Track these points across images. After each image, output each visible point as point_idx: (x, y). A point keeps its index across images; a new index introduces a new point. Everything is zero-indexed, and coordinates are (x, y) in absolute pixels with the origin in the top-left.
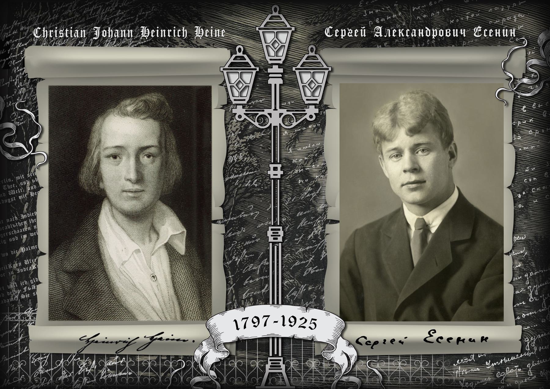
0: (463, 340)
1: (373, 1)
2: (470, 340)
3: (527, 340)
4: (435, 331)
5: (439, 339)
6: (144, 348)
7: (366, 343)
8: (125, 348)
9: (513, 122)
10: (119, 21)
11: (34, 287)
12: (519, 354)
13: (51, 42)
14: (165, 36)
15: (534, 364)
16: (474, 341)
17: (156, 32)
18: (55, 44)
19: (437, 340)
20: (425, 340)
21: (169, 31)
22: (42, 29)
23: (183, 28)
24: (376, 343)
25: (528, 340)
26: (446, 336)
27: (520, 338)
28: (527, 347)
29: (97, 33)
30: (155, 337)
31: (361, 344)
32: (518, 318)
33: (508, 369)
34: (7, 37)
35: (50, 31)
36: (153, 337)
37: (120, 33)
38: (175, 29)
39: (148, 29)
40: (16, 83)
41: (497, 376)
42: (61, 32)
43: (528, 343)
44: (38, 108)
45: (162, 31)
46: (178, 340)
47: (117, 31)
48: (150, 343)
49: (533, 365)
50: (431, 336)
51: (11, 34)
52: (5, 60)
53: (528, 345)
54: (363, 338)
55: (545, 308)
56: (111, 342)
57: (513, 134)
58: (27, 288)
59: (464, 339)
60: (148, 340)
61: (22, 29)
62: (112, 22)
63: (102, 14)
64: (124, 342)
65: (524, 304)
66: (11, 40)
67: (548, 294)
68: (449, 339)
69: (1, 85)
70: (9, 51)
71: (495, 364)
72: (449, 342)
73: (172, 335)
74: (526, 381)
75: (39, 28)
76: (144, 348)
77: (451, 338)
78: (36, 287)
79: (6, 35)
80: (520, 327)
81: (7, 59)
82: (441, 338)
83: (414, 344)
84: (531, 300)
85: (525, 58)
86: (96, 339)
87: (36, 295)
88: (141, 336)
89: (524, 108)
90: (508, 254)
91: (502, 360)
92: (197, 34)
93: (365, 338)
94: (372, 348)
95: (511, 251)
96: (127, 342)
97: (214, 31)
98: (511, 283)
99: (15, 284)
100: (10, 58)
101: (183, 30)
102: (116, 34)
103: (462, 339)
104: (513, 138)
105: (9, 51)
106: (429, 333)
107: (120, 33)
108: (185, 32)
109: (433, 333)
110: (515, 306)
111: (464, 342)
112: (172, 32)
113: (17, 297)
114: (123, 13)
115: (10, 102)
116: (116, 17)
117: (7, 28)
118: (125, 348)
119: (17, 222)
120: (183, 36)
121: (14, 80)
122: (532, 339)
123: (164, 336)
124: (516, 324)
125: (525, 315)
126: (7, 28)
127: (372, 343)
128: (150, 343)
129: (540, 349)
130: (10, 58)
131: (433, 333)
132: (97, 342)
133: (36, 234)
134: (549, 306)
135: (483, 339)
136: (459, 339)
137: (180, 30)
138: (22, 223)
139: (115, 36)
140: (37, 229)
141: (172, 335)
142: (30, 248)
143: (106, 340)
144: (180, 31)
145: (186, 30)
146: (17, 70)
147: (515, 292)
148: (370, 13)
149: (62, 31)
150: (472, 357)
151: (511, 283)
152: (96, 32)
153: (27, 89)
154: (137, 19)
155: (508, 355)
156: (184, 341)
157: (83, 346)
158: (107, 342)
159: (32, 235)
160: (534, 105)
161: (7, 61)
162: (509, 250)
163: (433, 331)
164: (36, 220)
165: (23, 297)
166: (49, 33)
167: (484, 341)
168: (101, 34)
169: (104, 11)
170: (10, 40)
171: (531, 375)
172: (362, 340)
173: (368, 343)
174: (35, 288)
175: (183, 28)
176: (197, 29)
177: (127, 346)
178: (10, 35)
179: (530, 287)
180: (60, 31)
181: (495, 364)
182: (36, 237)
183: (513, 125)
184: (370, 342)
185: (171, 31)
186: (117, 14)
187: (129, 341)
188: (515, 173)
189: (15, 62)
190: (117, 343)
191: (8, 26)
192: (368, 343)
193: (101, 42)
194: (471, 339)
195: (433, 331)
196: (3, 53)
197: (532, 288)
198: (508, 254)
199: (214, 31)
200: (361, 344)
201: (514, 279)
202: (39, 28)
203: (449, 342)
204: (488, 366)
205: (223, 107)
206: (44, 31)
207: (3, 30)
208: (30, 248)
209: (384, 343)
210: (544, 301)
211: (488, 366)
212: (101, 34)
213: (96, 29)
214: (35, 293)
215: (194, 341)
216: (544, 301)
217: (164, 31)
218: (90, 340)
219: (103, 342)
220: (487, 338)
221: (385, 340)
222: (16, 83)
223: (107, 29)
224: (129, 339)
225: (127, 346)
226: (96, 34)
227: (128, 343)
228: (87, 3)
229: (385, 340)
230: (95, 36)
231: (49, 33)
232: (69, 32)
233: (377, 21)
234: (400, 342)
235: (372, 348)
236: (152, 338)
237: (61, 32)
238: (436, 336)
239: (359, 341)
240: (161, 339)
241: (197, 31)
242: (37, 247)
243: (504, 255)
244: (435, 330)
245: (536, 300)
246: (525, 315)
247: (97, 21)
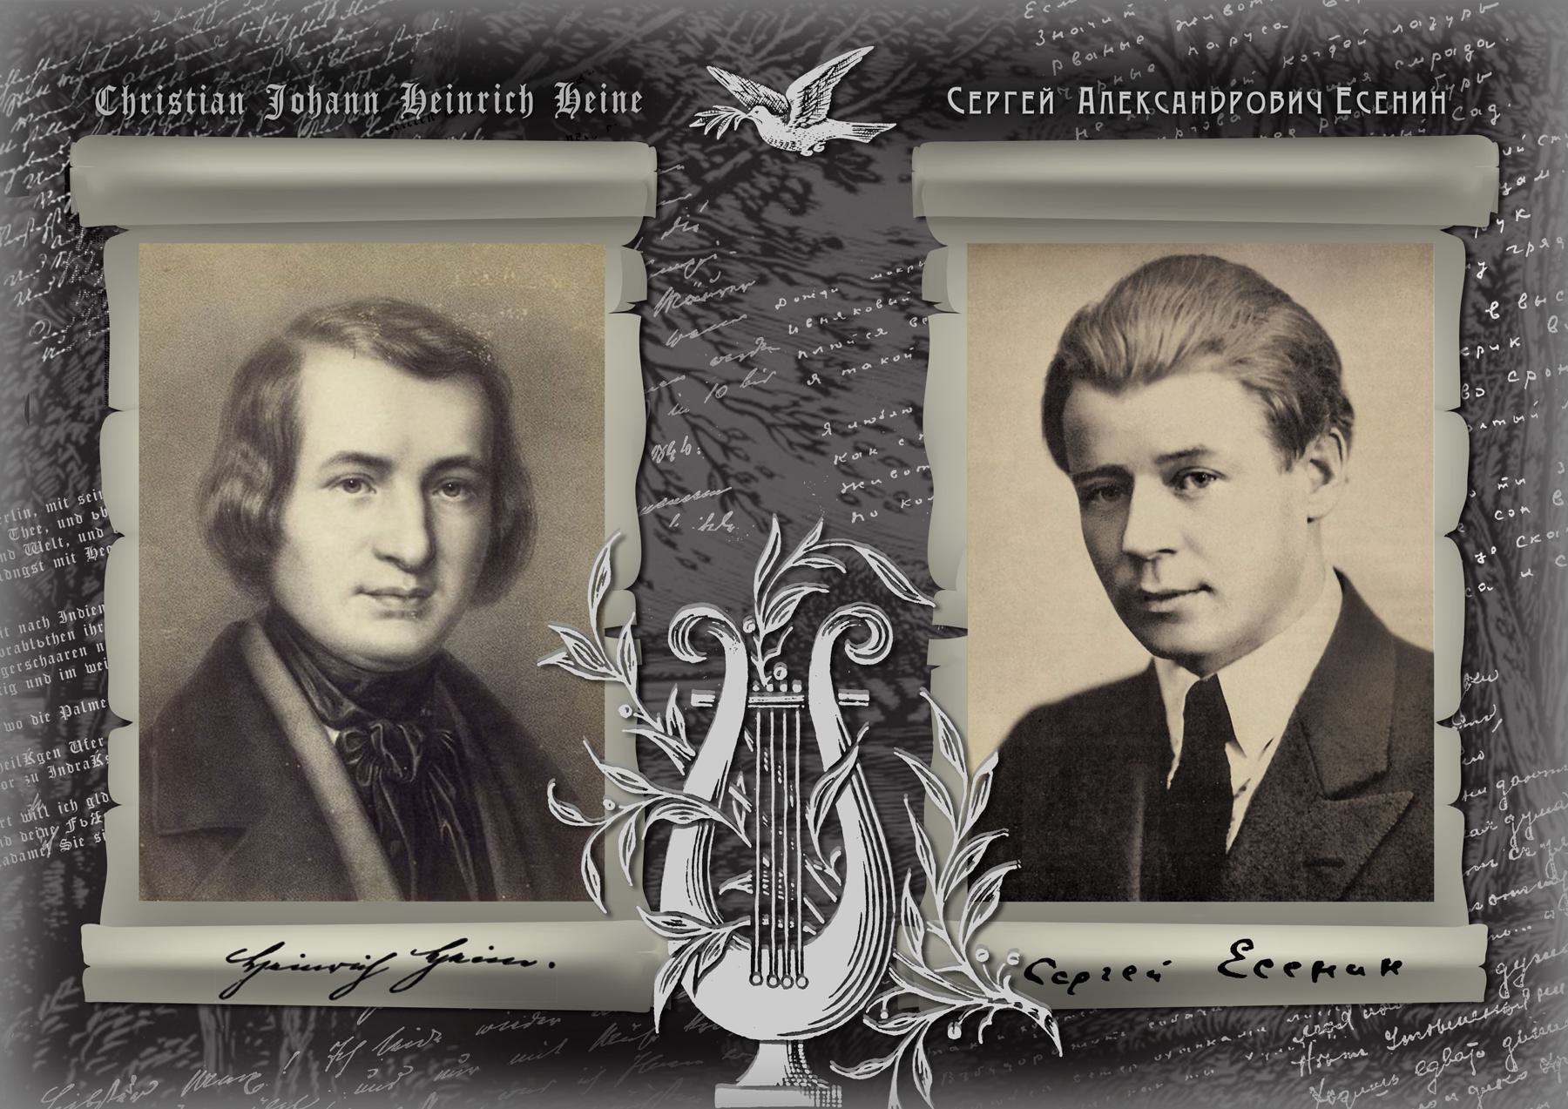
0: (1331, 970)
1: (1064, 4)
2: (1350, 969)
3: (1502, 968)
4: (1250, 945)
5: (1263, 968)
6: (411, 986)
7: (1055, 979)
8: (356, 983)
9: (1461, 348)
10: (340, 61)
11: (98, 817)
12: (1482, 1005)
13: (141, 125)
14: (469, 110)
15: (1523, 1039)
16: (1361, 971)
17: (444, 98)
18: (157, 125)
19: (1257, 969)
20: (1222, 968)
21: (481, 95)
22: (120, 91)
23: (523, 88)
24: (1083, 977)
25: (1505, 970)
26: (1281, 956)
27: (1482, 961)
28: (1503, 990)
29: (277, 102)
30: (442, 954)
31: (1038, 980)
32: (1479, 907)
33: (1447, 1052)
34: (19, 104)
35: (143, 96)
36: (436, 953)
37: (341, 101)
38: (499, 91)
39: (421, 92)
40: (45, 236)
41: (1417, 1072)
42: (174, 99)
43: (1506, 978)
44: (107, 308)
45: (461, 95)
46: (507, 961)
47: (335, 95)
48: (429, 969)
49: (1520, 1041)
50: (1239, 957)
51: (31, 95)
52: (13, 171)
53: (1505, 983)
54: (1046, 964)
55: (1554, 877)
56: (318, 968)
57: (1462, 384)
58: (77, 820)
59: (1333, 968)
60: (423, 962)
61: (62, 82)
62: (320, 63)
63: (290, 39)
64: (355, 966)
65: (1493, 865)
66: (32, 115)
67: (1563, 839)
68: (1290, 968)
69: (4, 241)
70: (26, 144)
71: (1412, 1038)
72: (1291, 975)
73: (491, 948)
74: (1499, 1087)
75: (112, 89)
76: (411, 986)
77: (1296, 965)
78: (102, 819)
79: (17, 99)
80: (1481, 929)
81: (20, 168)
82: (1268, 963)
83: (1192, 977)
84: (1515, 854)
85: (1497, 170)
86: (273, 958)
87: (103, 842)
88: (404, 954)
89: (1493, 308)
90: (1447, 723)
91: (1431, 1027)
92: (560, 104)
93: (1052, 963)
94: (1070, 992)
95: (1456, 716)
96: (361, 968)
97: (609, 96)
98: (1459, 804)
99: (42, 811)
100: (27, 164)
101: (522, 93)
102: (331, 106)
103: (1326, 966)
104: (1463, 394)
105: (26, 144)
106: (1234, 949)
107: (341, 101)
108: (527, 99)
109: (1244, 949)
110: (1468, 873)
111: (1363, 974)
112: (492, 98)
113: (48, 846)
114: (350, 37)
115: (30, 292)
116: (333, 47)
117: (21, 80)
118: (356, 983)
119: (48, 632)
120: (523, 110)
121: (39, 229)
122: (1516, 967)
123: (467, 951)
124: (1471, 922)
125: (1496, 899)
126: (21, 80)
127: (1071, 979)
128: (429, 969)
129: (1540, 996)
130: (27, 164)
131: (1244, 949)
132: (276, 967)
133: (103, 666)
134: (1566, 873)
135: (1388, 966)
136: (1318, 967)
137: (512, 94)
138: (62, 635)
139: (328, 111)
140: (104, 654)
141: (491, 948)
142: (87, 708)
143: (303, 962)
144: (513, 95)
145: (530, 94)
146: (47, 200)
147: (1467, 833)
148: (1054, 37)
149: (178, 96)
150: (1345, 1017)
151: (1459, 804)
152: (275, 99)
153: (78, 253)
154: (391, 54)
155: (1451, 1009)
156: (525, 963)
157: (237, 980)
158: (306, 968)
159: (91, 669)
160: (1521, 301)
161: (19, 173)
162: (1452, 713)
163: (1245, 945)
164: (103, 628)
165: (65, 846)
166: (139, 104)
167: (1390, 972)
168: (287, 103)
169: (297, 32)
170: (28, 113)
171: (1515, 1069)
172: (1042, 970)
173: (1059, 978)
174: (98, 821)
175: (523, 88)
176: (562, 91)
177: (363, 977)
178: (29, 99)
179: (1511, 817)
180: (171, 98)
181: (1412, 1038)
182: (103, 676)
183: (1461, 356)
184: (1064, 974)
185: (487, 95)
186: (334, 41)
187: (368, 963)
188: (1469, 492)
189: (42, 178)
190: (332, 968)
191: (22, 75)
192: (1059, 978)
193: (288, 127)
194: (1354, 966)
195: (1245, 945)
196: (7, 150)
197: (1516, 822)
198: (1447, 723)
199: (609, 96)
200: (1038, 980)
201: (1466, 796)
202: (112, 89)
203: (1291, 975)
204: (1391, 1043)
205: (637, 308)
206: (125, 95)
207: (7, 86)
208: (87, 708)
209: (1105, 978)
210: (1551, 860)
211: (1391, 1043)
212: (287, 103)
213: (273, 91)
214: (101, 836)
215: (552, 965)
216: (1551, 860)
217: (469, 95)
218: (256, 962)
219: (295, 967)
220: (1398, 964)
221: (1107, 970)
222: (45, 236)
223: (304, 91)
224: (368, 957)
225: (363, 977)
226: (275, 105)
227: (365, 971)
228: (249, 8)
229: (1107, 970)
230: (272, 112)
231: (139, 104)
232: (196, 100)
233: (1074, 59)
234: (1151, 974)
235: (1070, 992)
236: (433, 957)
237: (174, 99)
238: (1252, 957)
239: (1035, 971)
240: (458, 958)
241: (560, 97)
242: (107, 704)
243: (1437, 727)
244: (1249, 942)
245: (1528, 854)
246: (1496, 899)
247: (277, 62)
